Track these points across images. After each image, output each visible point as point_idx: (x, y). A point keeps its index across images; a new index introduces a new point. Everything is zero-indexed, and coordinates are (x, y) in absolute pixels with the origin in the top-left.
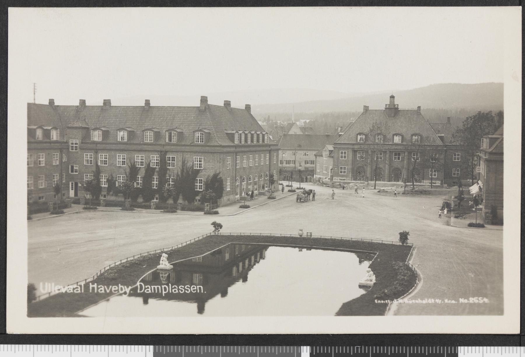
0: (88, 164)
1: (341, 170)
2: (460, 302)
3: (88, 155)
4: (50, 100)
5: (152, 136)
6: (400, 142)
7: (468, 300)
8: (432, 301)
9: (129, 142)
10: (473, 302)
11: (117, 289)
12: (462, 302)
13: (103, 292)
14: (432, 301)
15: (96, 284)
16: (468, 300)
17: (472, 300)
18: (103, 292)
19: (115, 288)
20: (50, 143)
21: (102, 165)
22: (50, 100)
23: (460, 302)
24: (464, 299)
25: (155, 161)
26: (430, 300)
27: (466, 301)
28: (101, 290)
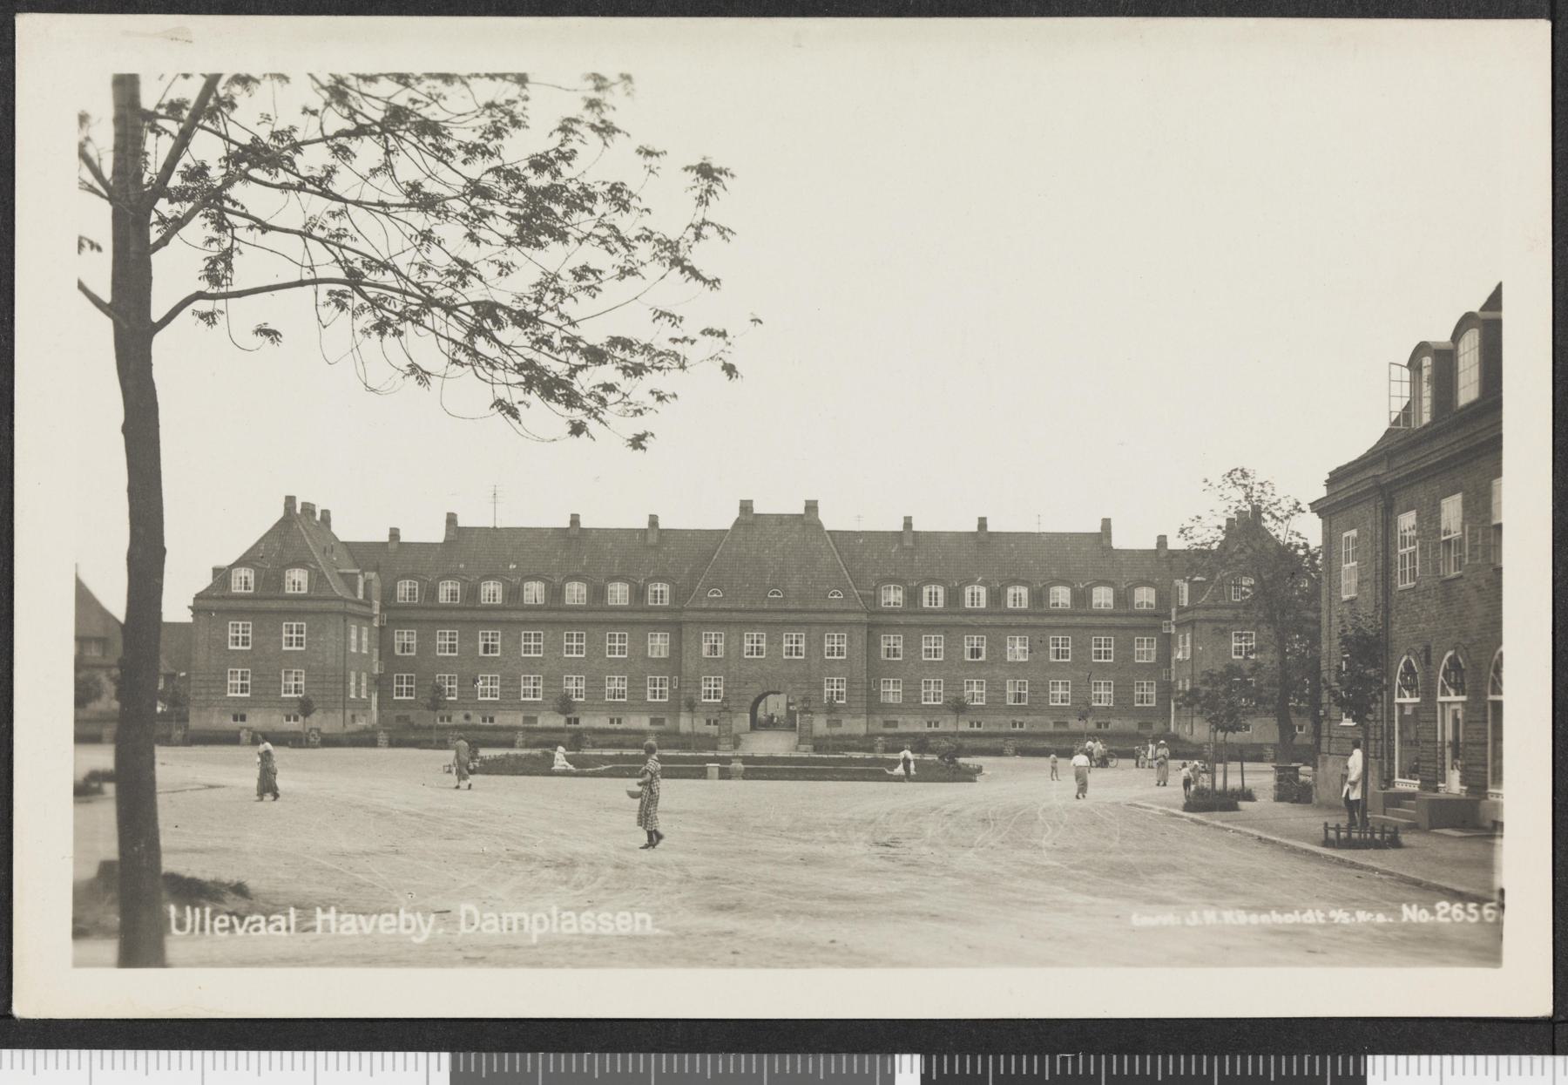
0: (1058, 658)
1: (528, 643)
2: (1405, 919)
3: (238, 625)
4: (391, 529)
5: (583, 596)
6: (625, 601)
7: (1433, 912)
8: (1316, 917)
9: (1116, 611)
10: (1447, 920)
11: (394, 922)
12: (1410, 920)
13: (354, 931)
14: (1316, 917)
15: (333, 910)
16: (1433, 912)
17: (1445, 911)
18: (354, 931)
19: (388, 920)
20: (1002, 614)
21: (237, 648)
22: (391, 529)
23: (1405, 919)
24: (1419, 909)
25: (836, 645)
26: (1310, 913)
27: (1424, 916)
28: (348, 929)
